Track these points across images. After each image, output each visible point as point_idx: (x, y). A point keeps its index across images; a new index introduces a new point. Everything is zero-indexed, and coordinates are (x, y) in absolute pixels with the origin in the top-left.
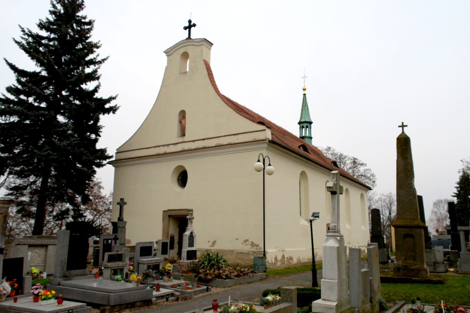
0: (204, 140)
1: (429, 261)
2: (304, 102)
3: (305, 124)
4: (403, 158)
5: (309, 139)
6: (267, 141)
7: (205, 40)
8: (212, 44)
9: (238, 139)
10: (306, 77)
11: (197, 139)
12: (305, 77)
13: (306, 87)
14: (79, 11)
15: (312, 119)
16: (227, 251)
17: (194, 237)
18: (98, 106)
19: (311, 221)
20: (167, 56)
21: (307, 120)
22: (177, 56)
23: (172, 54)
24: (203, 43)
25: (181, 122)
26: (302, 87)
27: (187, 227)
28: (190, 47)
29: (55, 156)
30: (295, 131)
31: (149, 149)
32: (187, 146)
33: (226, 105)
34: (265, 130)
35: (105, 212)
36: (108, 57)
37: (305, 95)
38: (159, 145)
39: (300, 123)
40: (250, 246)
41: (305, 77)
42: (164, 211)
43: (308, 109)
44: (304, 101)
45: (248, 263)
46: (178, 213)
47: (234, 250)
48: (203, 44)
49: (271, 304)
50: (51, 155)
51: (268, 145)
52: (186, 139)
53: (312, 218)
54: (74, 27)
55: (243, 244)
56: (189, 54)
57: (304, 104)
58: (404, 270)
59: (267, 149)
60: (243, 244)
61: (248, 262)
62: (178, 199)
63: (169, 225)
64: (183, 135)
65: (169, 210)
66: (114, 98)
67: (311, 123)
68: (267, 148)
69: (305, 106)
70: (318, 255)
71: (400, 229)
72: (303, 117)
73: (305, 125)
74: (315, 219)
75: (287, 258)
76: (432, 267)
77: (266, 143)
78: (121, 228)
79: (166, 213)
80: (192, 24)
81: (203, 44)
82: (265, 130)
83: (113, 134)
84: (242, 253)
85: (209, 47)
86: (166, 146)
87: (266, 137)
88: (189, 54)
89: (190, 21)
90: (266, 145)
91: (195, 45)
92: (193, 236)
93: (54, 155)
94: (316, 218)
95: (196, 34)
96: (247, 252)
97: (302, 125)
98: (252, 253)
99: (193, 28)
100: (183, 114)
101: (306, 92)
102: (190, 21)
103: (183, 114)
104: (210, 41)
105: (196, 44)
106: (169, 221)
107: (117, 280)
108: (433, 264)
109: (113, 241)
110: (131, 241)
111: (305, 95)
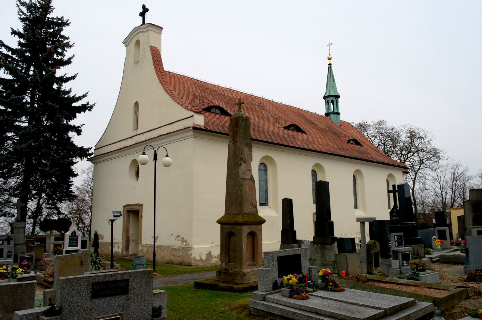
0: (150, 131)
1: (329, 260)
2: (329, 73)
3: (332, 98)
4: (234, 142)
5: (336, 115)
6: (191, 128)
7: (150, 25)
8: (162, 28)
9: (173, 128)
10: (327, 46)
12: (329, 45)
13: (332, 55)
14: (49, 12)
15: (340, 92)
16: (165, 246)
17: (78, 236)
18: (68, 107)
19: (112, 221)
20: (126, 46)
21: (332, 93)
22: (132, 45)
23: (129, 44)
24: (149, 28)
26: (328, 56)
27: (70, 226)
28: (141, 34)
29: (14, 159)
30: (319, 108)
31: (115, 144)
33: (165, 93)
34: (192, 116)
36: (74, 55)
37: (330, 65)
39: (325, 97)
40: (181, 242)
41: (329, 45)
43: (334, 81)
44: (329, 71)
45: (179, 260)
47: (170, 246)
48: (149, 30)
50: (11, 158)
51: (194, 132)
52: (139, 131)
53: (112, 218)
55: (176, 239)
56: (143, 43)
57: (329, 76)
58: (224, 273)
59: (194, 136)
60: (176, 239)
61: (178, 258)
63: (129, 220)
65: (127, 205)
66: (84, 96)
67: (338, 97)
68: (194, 136)
69: (330, 77)
70: (192, 255)
71: (225, 226)
72: (328, 91)
73: (330, 99)
74: (116, 219)
76: (332, 267)
77: (190, 131)
78: (18, 229)
81: (149, 30)
82: (192, 116)
83: (89, 130)
84: (174, 249)
85: (159, 31)
86: (125, 140)
87: (194, 124)
88: (143, 43)
90: (191, 133)
91: (143, 32)
92: (77, 235)
93: (14, 157)
94: (117, 218)
95: (150, 18)
96: (178, 248)
97: (327, 99)
98: (181, 249)
101: (331, 62)
102: (144, 7)
104: (160, 26)
105: (145, 30)
106: (129, 217)
108: (332, 263)
110: (104, 236)
111: (330, 65)
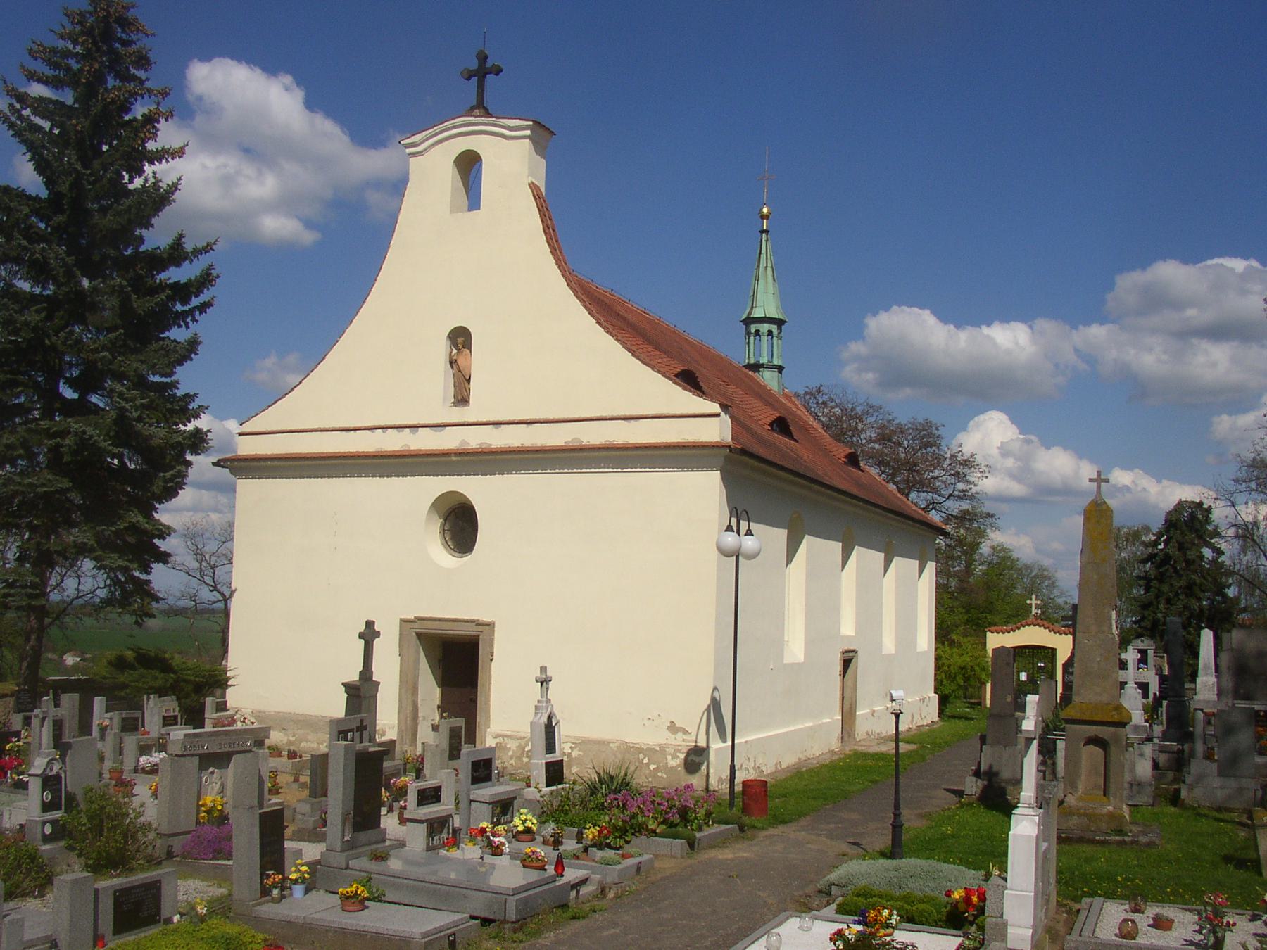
11: (506, 419)
25: (453, 362)
32: (475, 439)
34: (718, 415)
35: (1216, 938)
38: (382, 424)
42: (403, 621)
46: (449, 630)
49: (285, 753)
54: (1212, 258)
62: (451, 589)
64: (462, 399)
75: (149, 582)
79: (412, 625)
80: (489, 64)
82: (718, 415)
89: (483, 58)
99: (490, 78)
100: (460, 338)
102: (483, 58)
103: (460, 338)
107: (343, 836)
109: (357, 735)
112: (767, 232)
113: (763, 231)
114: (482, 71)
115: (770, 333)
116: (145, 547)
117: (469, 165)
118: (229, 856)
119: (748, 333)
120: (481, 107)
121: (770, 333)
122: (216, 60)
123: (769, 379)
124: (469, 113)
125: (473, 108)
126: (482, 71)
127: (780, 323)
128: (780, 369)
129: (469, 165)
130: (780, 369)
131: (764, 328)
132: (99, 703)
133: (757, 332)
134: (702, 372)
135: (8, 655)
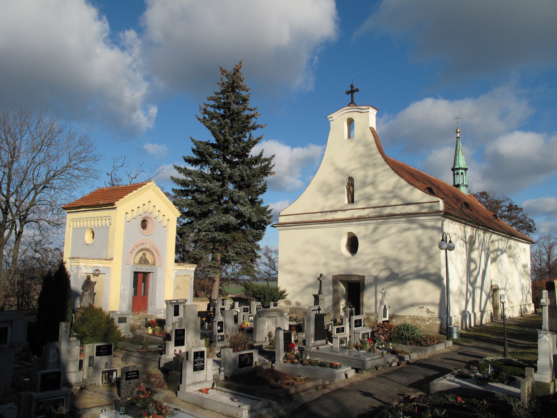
89: (352, 86)
102: (352, 86)
112: (459, 138)
113: (457, 138)
114: (352, 91)
115: (462, 173)
116: (252, 256)
117: (350, 122)
118: (361, 320)
119: (454, 175)
120: (352, 103)
121: (462, 173)
122: (269, 141)
123: (463, 190)
124: (349, 105)
125: (350, 104)
126: (352, 91)
127: (466, 169)
128: (466, 186)
129: (350, 122)
130: (466, 186)
131: (461, 171)
132: (237, 304)
133: (458, 174)
134: (435, 190)
135: (3, 153)
